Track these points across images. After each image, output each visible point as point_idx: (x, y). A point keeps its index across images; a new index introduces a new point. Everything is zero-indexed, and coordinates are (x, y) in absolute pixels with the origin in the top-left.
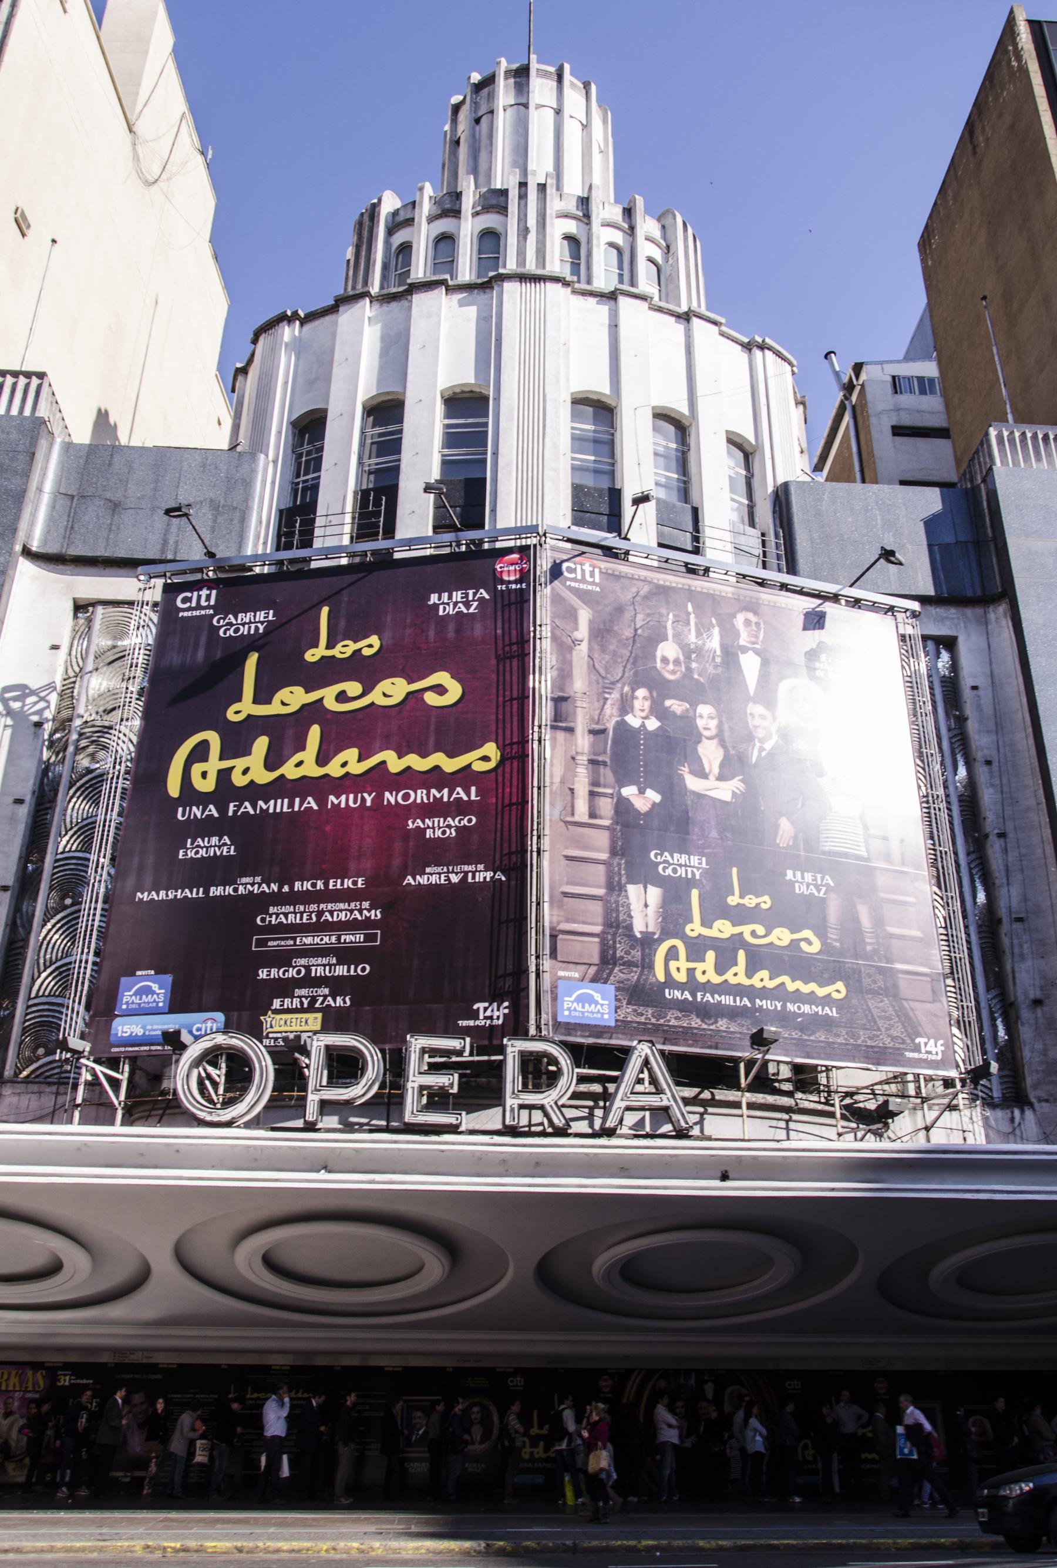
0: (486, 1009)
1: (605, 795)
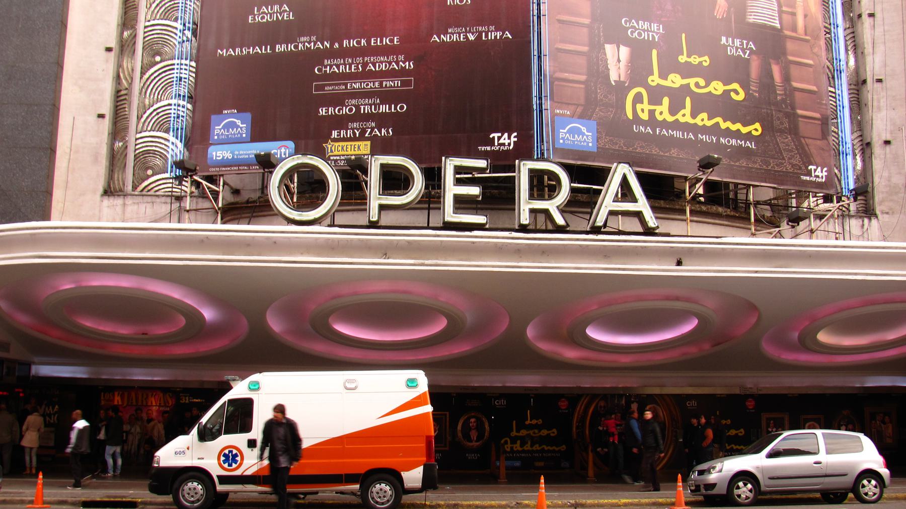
0: (499, 138)
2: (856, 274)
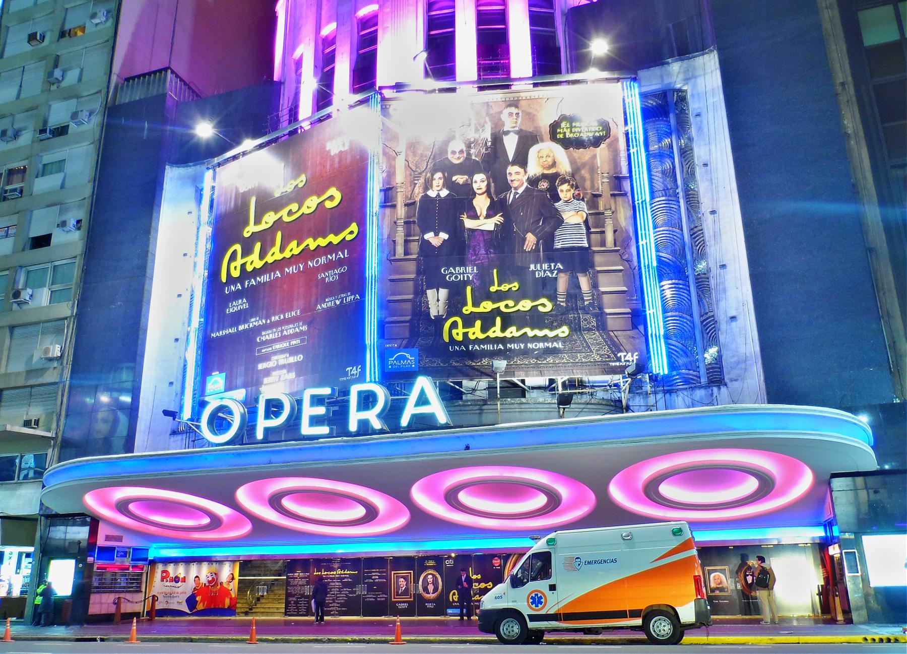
0: (625, 356)
1: (414, 241)
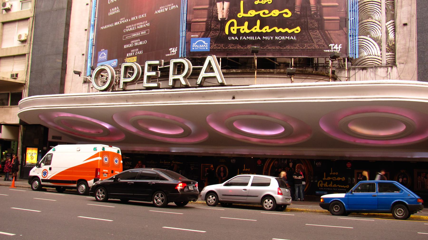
0: (333, 46)
2: (315, 99)
